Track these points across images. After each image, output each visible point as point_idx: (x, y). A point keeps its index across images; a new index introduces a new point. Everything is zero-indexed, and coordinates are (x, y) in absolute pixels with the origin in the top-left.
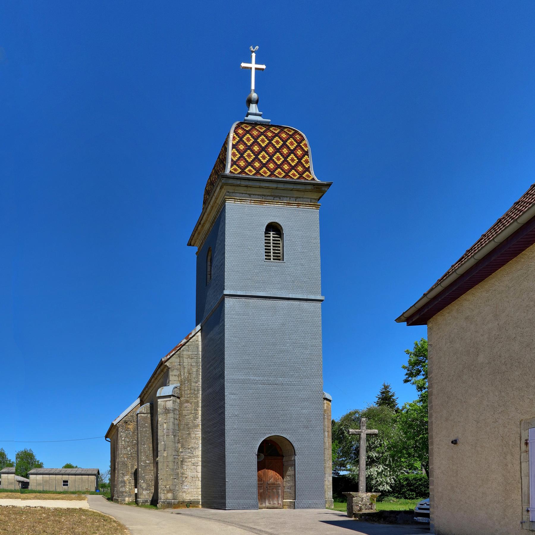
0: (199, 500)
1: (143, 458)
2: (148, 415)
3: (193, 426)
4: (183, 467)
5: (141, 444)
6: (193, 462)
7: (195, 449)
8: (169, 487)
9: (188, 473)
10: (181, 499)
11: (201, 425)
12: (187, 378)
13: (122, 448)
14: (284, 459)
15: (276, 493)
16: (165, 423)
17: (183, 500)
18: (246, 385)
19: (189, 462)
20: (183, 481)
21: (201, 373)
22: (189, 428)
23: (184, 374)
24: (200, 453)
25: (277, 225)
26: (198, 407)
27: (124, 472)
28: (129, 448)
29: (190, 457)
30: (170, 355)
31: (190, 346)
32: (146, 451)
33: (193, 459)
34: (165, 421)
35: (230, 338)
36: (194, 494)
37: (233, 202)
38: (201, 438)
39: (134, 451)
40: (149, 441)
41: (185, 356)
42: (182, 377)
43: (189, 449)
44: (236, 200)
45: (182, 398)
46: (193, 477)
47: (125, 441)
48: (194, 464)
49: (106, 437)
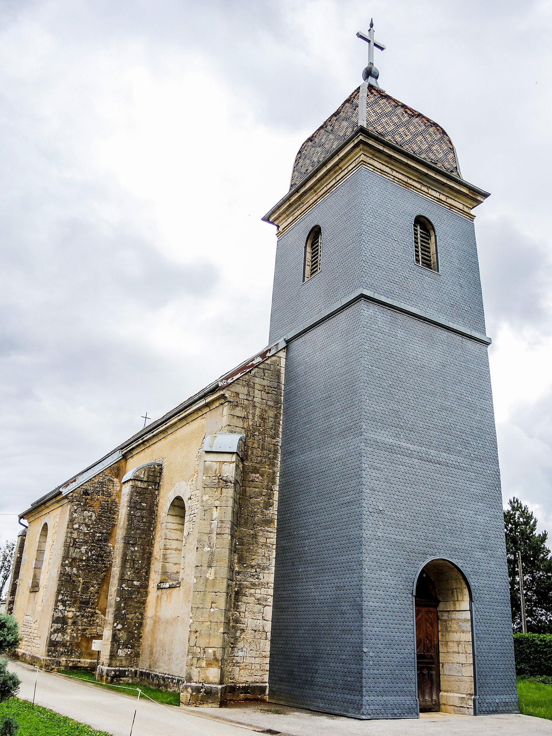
0: (264, 685)
1: (129, 573)
2: (149, 486)
3: (263, 521)
4: (238, 605)
5: (129, 544)
6: (258, 596)
7: (264, 569)
8: (214, 653)
9: (246, 620)
10: (230, 681)
11: (276, 521)
12: (258, 425)
13: (71, 545)
14: (441, 606)
15: (427, 677)
16: (216, 507)
17: (233, 682)
18: (395, 455)
19: (251, 595)
20: (237, 639)
21: (281, 422)
22: (255, 524)
23: (254, 417)
24: (271, 578)
25: (427, 222)
26: (274, 483)
27: (66, 598)
28: (86, 547)
29: (253, 584)
30: (233, 379)
31: (266, 371)
32: (136, 559)
33: (258, 591)
34: (217, 503)
35: (370, 367)
36: (256, 670)
37: (372, 170)
38: (274, 547)
39: (93, 555)
40: (145, 538)
41: (257, 386)
42: (251, 423)
43: (252, 567)
44: (376, 169)
45: (246, 463)
46: (255, 631)
47: (78, 532)
48: (259, 601)
49: (21, 517)
